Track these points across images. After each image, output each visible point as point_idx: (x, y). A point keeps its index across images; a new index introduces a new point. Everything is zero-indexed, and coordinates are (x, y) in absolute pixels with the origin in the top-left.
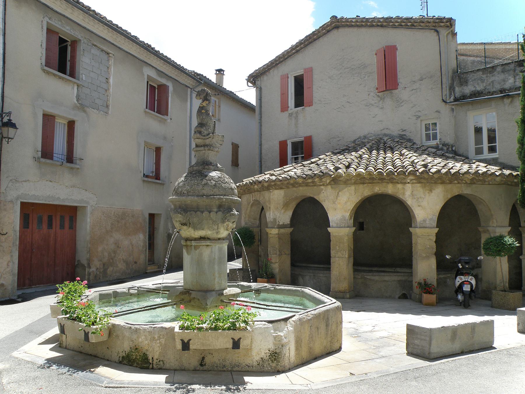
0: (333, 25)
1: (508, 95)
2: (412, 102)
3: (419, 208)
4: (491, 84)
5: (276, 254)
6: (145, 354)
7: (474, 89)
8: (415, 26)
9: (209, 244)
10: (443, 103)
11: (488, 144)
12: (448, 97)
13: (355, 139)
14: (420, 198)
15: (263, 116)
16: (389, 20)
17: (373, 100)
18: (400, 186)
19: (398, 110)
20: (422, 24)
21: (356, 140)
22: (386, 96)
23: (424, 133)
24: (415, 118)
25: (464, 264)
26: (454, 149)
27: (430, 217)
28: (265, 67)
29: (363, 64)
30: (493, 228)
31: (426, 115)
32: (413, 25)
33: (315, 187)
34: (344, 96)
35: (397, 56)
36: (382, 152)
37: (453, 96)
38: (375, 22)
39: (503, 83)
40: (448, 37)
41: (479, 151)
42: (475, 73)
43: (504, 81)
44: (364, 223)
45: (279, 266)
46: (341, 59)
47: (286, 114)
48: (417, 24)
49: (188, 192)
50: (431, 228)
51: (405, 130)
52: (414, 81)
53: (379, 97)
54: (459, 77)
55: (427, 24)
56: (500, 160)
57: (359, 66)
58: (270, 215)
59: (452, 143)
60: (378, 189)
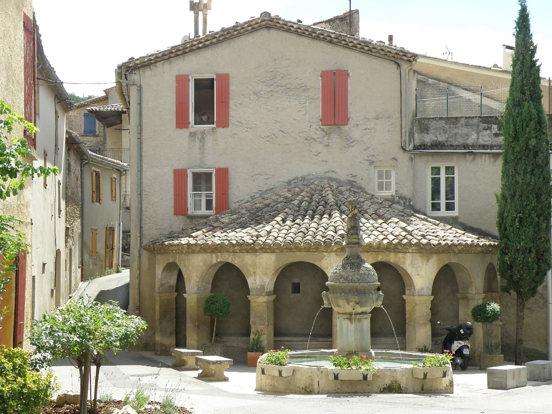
1: (472, 152)
2: (365, 144)
5: (264, 325)
7: (436, 139)
9: (367, 317)
11: (197, 81)
12: (407, 145)
15: (144, 128)
17: (316, 134)
18: (401, 255)
20: (382, 52)
21: (291, 181)
23: (376, 181)
25: (466, 330)
26: (411, 203)
27: (427, 285)
28: (152, 58)
29: (303, 85)
30: (472, 295)
31: (381, 161)
34: (276, 122)
37: (413, 143)
39: (466, 138)
40: (410, 73)
41: (436, 207)
42: (437, 121)
43: (467, 135)
47: (185, 132)
48: (376, 50)
49: (359, 280)
52: (368, 119)
53: (324, 131)
54: (419, 122)
55: (388, 54)
56: (460, 220)
57: (298, 87)
58: (255, 281)
59: (409, 197)
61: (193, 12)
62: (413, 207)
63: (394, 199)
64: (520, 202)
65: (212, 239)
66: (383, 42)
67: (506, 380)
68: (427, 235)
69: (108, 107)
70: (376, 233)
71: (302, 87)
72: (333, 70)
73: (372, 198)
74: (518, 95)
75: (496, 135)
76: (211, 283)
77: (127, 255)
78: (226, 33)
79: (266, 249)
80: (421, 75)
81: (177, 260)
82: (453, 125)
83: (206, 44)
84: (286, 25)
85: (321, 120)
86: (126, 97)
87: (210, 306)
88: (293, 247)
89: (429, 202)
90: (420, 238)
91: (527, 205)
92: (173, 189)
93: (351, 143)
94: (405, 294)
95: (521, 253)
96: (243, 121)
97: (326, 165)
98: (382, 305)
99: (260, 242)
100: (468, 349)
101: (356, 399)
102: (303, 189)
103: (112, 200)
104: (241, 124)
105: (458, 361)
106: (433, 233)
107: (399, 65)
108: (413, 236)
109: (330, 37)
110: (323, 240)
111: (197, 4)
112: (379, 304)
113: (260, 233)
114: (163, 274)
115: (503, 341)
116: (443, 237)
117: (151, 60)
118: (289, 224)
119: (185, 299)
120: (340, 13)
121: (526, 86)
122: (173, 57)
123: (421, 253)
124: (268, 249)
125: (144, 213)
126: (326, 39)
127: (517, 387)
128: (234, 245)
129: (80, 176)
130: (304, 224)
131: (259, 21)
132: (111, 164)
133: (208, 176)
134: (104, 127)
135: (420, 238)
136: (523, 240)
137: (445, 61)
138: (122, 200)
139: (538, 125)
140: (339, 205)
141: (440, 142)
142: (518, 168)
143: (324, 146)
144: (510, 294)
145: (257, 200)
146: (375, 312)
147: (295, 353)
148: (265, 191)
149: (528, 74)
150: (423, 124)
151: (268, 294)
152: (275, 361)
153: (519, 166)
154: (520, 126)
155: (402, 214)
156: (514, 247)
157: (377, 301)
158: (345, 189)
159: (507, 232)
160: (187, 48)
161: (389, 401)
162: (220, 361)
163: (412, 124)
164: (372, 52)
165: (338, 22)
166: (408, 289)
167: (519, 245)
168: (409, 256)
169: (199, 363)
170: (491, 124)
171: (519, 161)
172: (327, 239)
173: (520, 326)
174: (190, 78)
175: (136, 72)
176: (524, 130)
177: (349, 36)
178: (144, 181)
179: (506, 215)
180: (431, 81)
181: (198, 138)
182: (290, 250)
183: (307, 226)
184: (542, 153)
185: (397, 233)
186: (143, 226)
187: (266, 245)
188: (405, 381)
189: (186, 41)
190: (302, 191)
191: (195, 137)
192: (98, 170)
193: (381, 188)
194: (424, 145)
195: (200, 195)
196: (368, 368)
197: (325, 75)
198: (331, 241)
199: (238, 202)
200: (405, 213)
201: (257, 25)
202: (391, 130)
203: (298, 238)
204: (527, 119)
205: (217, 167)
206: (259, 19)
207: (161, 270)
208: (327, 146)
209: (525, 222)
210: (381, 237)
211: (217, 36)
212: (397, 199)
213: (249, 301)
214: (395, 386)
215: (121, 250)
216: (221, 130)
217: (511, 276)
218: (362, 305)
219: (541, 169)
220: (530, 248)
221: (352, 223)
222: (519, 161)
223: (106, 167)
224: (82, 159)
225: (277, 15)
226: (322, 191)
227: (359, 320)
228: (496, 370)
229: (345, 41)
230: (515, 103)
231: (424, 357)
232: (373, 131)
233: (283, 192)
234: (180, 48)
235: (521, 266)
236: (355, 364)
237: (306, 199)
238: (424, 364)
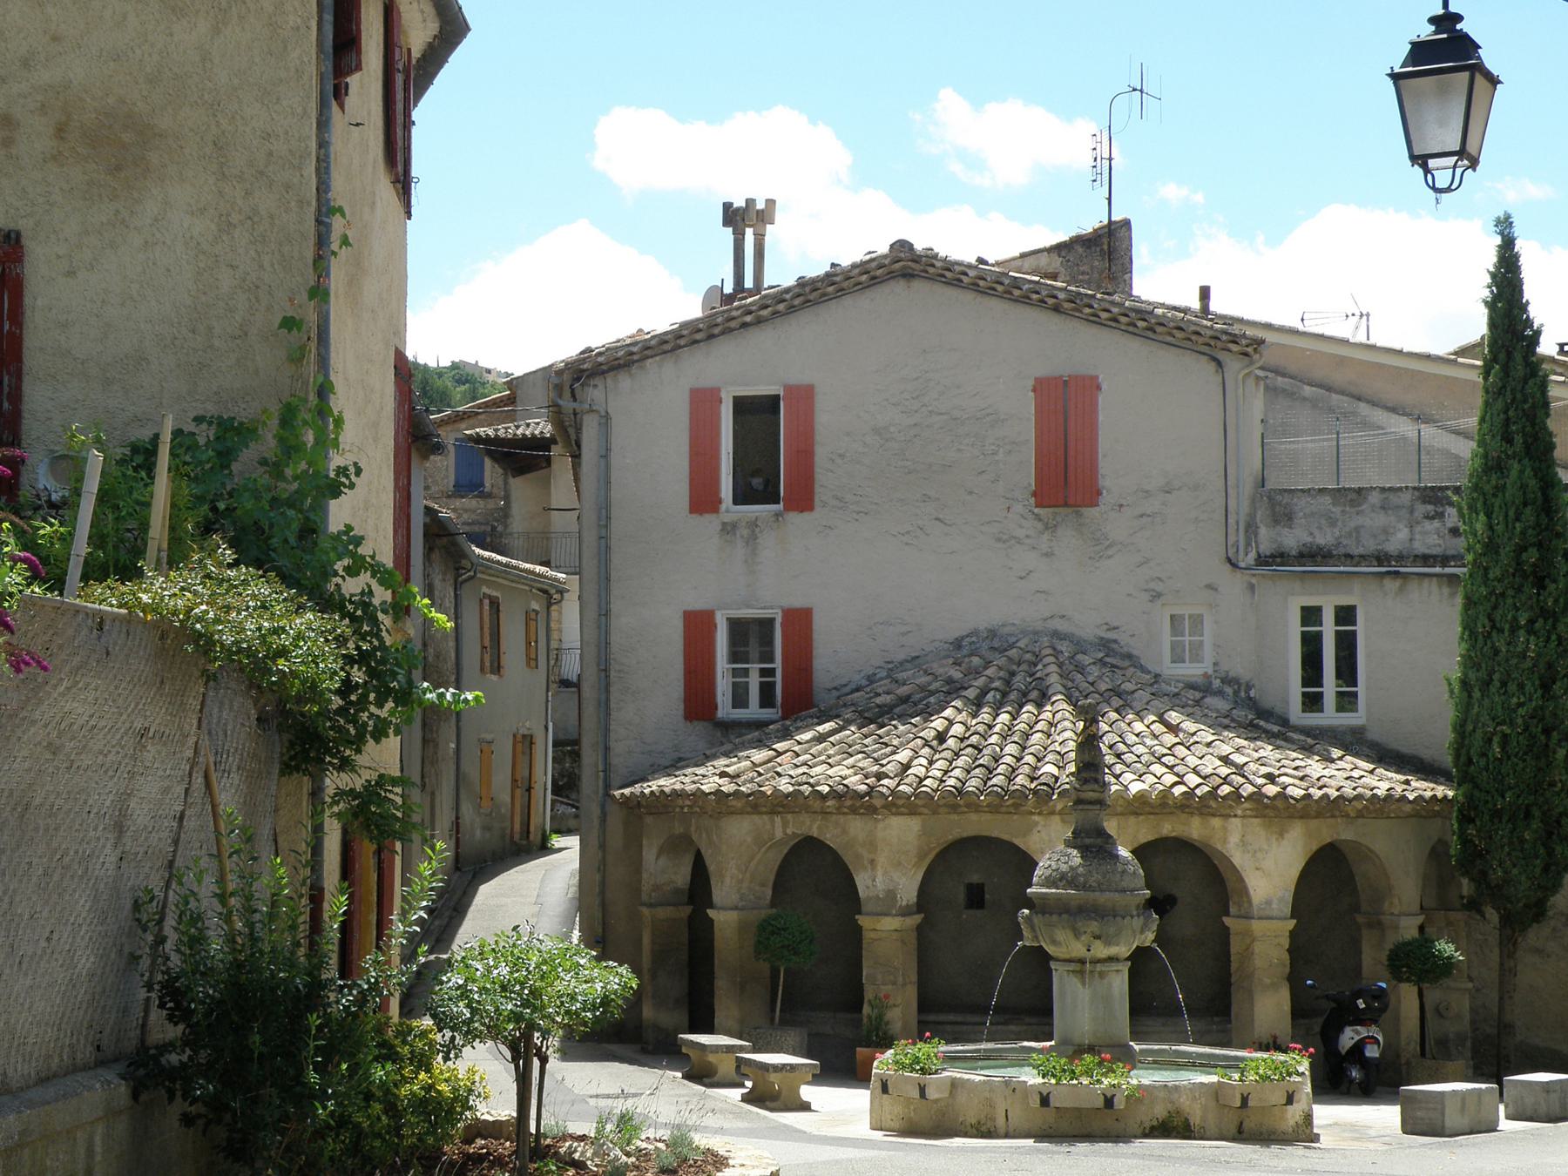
1: (1397, 573)
2: (1139, 551)
4: (1354, 535)
6: (1187, 1120)
7: (1310, 539)
9: (1120, 968)
10: (1228, 565)
13: (957, 634)
14: (1260, 850)
17: (1021, 527)
18: (1216, 822)
19: (1096, 568)
20: (1179, 334)
21: (963, 638)
22: (1063, 520)
26: (1252, 693)
28: (635, 349)
29: (990, 411)
31: (1178, 591)
32: (1151, 329)
33: (1015, 817)
35: (1100, 408)
37: (1254, 551)
39: (1382, 537)
41: (1313, 702)
44: (986, 889)
46: (917, 379)
50: (1280, 919)
51: (1117, 628)
52: (1147, 492)
53: (1040, 520)
54: (1269, 498)
55: (1194, 337)
56: (1373, 735)
58: (874, 880)
60: (1170, 827)
61: (731, 229)
62: (1255, 703)
63: (1211, 683)
64: (1503, 697)
65: (773, 783)
67: (1443, 1114)
68: (1279, 776)
69: (517, 427)
70: (1157, 769)
71: (988, 415)
72: (1062, 376)
73: (1155, 682)
74: (1496, 445)
75: (1455, 532)
76: (771, 884)
77: (562, 802)
78: (807, 289)
79: (899, 805)
80: (1284, 375)
81: (693, 829)
82: (1352, 506)
83: (763, 316)
84: (949, 270)
85: (1035, 494)
86: (571, 431)
87: (768, 939)
88: (962, 803)
89: (1296, 690)
90: (1261, 781)
91: (1520, 705)
94: (1227, 914)
95: (1505, 818)
98: (1153, 941)
99: (884, 790)
100: (1376, 1047)
101: (1083, 1147)
102: (991, 659)
103: (528, 665)
104: (842, 504)
105: (1354, 1074)
106: (1296, 768)
107: (1219, 364)
108: (1247, 779)
109: (1055, 297)
110: (1033, 786)
111: (741, 212)
112: (1148, 938)
113: (884, 769)
115: (1477, 1029)
116: (1318, 779)
117: (632, 354)
118: (953, 747)
119: (712, 921)
121: (1514, 423)
122: (684, 346)
123: (1265, 816)
124: (903, 806)
125: (614, 714)
126: (1046, 303)
127: (1471, 1133)
128: (823, 797)
129: (453, 611)
130: (989, 748)
132: (526, 578)
133: (766, 624)
134: (506, 474)
135: (1261, 781)
136: (1510, 788)
137: (1345, 342)
138: (552, 662)
139: (1543, 516)
140: (1073, 700)
141: (1320, 548)
142: (1498, 615)
144: (1483, 916)
145: (881, 686)
146: (1140, 957)
147: (962, 1048)
148: (901, 663)
149: (1519, 396)
150: (1280, 504)
151: (905, 912)
152: (911, 1065)
153: (1501, 612)
154: (1501, 519)
155: (1226, 721)
156: (1490, 806)
157: (1142, 932)
158: (1091, 661)
159: (1473, 767)
160: (716, 325)
161: (1158, 1153)
162: (791, 1065)
163: (1253, 501)
164: (1155, 332)
165: (1080, 250)
166: (1234, 903)
167: (1500, 799)
168: (1235, 823)
169: (744, 1069)
170: (1442, 505)
171: (1500, 600)
172: (1040, 784)
173: (1508, 992)
174: (723, 395)
175: (598, 381)
176: (1510, 526)
177: (1099, 296)
179: (1470, 727)
180: (1308, 390)
181: (742, 537)
182: (954, 808)
183: (995, 752)
184: (1555, 581)
185: (1209, 771)
186: (612, 744)
187: (899, 798)
188: (1199, 1113)
189: (714, 308)
190: (987, 664)
191: (735, 534)
192: (495, 594)
193: (1178, 658)
194: (1282, 555)
195: (746, 672)
196: (1116, 1082)
197: (1043, 388)
198: (1049, 790)
199: (835, 688)
200: (1233, 720)
201: (881, 271)
203: (974, 782)
204: (1517, 501)
206: (885, 257)
207: (655, 851)
209: (1515, 744)
210: (1170, 779)
211: (788, 296)
212: (1217, 683)
213: (860, 928)
214: (1177, 1121)
215: (549, 791)
216: (794, 518)
217: (1484, 874)
218: (1108, 943)
219: (1551, 620)
220: (1528, 808)
221: (1087, 756)
222: (1500, 600)
223: (514, 585)
224: (457, 569)
225: (928, 247)
226: (1036, 665)
227: (1102, 975)
228: (1420, 1091)
229: (1091, 307)
230: (1490, 463)
231: (1242, 1059)
233: (942, 666)
234: (701, 326)
235: (1507, 849)
236: (1089, 1073)
237: (997, 684)
238: (1242, 1075)
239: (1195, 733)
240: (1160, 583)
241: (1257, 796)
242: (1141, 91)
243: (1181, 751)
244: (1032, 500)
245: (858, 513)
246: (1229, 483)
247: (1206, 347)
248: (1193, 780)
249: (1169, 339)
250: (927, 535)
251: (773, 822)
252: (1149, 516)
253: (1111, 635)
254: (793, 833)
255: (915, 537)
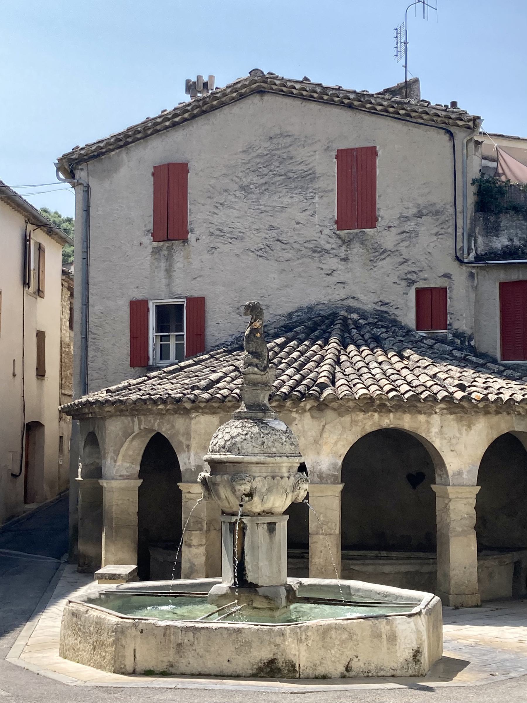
0: (254, 86)
2: (401, 255)
3: (452, 453)
7: (509, 243)
8: (411, 117)
10: (457, 262)
13: (290, 311)
14: (454, 437)
15: (91, 245)
16: (367, 99)
17: (329, 243)
18: (422, 418)
19: (375, 267)
20: (425, 117)
24: (404, 283)
26: (472, 343)
28: (102, 145)
29: (310, 172)
36: (492, 397)
37: (474, 252)
38: (338, 97)
45: (206, 551)
46: (266, 155)
48: (417, 114)
52: (406, 217)
55: (435, 118)
58: (189, 459)
66: (426, 102)
71: (309, 175)
83: (176, 122)
85: (337, 222)
92: (129, 330)
93: (381, 254)
96: (226, 229)
97: (344, 288)
104: (222, 234)
114: (87, 451)
120: (392, 84)
125: (90, 364)
131: (247, 83)
143: (341, 260)
168: (436, 419)
175: (83, 166)
178: (91, 319)
186: (89, 382)
191: (160, 254)
202: (440, 233)
205: (188, 295)
208: (345, 260)
213: (181, 492)
229: (371, 103)
232: (413, 235)
234: (139, 129)
239: (418, 362)
240: (414, 275)
241: (449, 399)
242: (424, 3)
243: (405, 372)
244: (335, 226)
245: (231, 238)
246: (457, 210)
247: (444, 125)
248: (405, 388)
249: (420, 121)
250: (272, 250)
251: (133, 422)
252: (408, 233)
253: (384, 308)
254: (144, 428)
255: (266, 252)
